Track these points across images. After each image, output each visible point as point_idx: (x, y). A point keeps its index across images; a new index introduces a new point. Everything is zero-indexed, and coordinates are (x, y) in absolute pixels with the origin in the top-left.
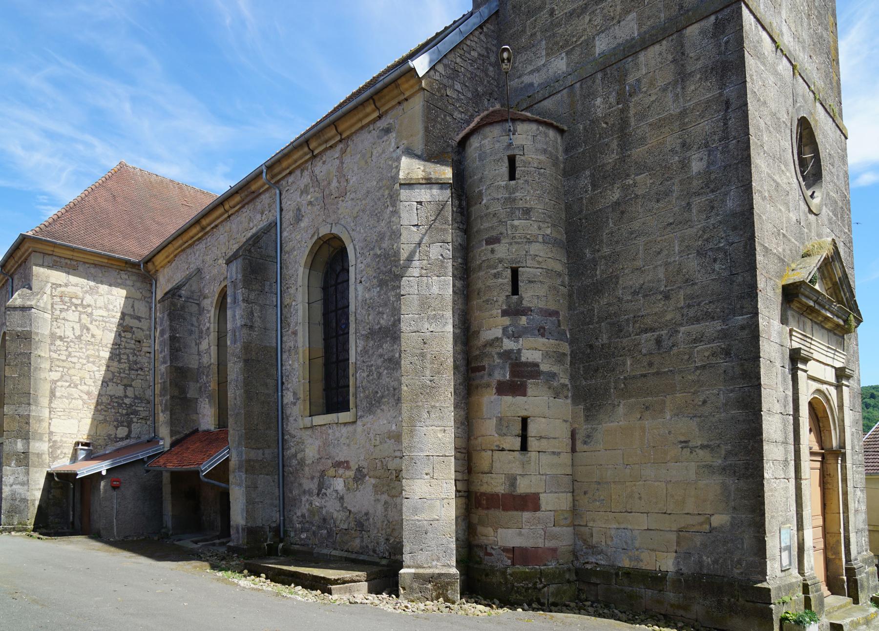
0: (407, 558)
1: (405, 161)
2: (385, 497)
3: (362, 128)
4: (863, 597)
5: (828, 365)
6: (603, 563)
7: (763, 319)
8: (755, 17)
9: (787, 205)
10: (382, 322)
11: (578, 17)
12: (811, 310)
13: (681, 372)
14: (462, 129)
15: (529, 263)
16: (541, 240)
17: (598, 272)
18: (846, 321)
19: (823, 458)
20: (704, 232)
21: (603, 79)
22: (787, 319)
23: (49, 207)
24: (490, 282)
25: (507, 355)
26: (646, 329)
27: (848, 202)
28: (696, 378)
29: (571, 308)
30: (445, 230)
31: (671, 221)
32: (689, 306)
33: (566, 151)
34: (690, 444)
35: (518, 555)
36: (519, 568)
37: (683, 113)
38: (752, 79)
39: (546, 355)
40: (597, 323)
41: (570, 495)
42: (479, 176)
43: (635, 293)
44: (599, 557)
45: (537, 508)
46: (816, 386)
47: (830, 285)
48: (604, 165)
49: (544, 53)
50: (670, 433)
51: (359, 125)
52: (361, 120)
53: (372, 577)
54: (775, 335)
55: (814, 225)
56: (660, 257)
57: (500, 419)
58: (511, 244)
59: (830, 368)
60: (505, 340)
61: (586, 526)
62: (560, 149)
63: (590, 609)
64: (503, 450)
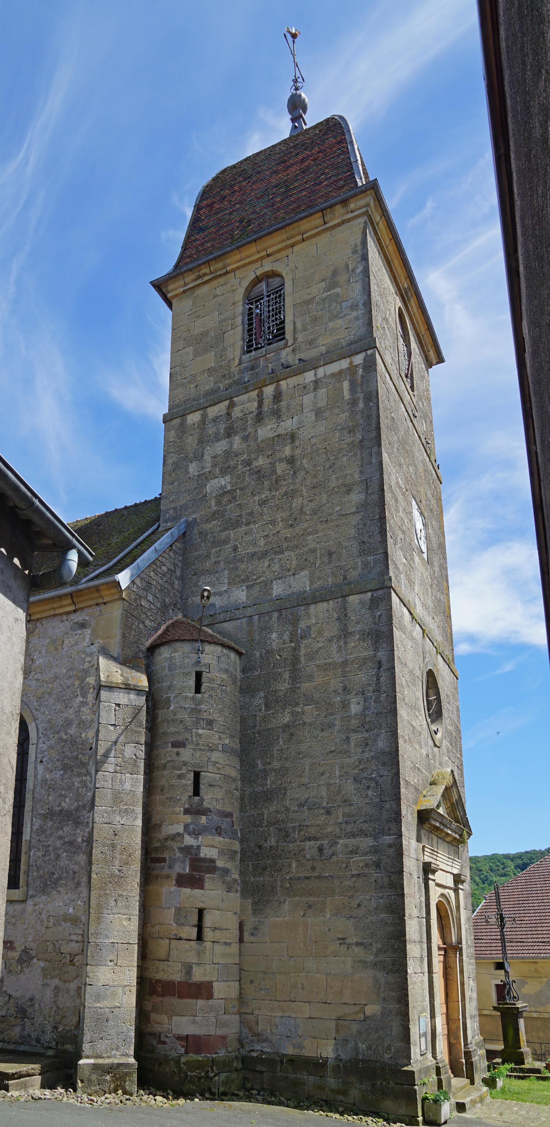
0: (86, 1047)
1: (103, 661)
2: (56, 981)
3: (54, 616)
4: (478, 1078)
5: (448, 872)
6: (268, 1050)
7: (405, 839)
8: (399, 598)
9: (420, 743)
10: (63, 804)
11: (259, 560)
12: (437, 829)
13: (339, 878)
14: (151, 635)
15: (211, 768)
16: (221, 749)
17: (268, 782)
18: (461, 835)
19: (445, 952)
20: (360, 762)
21: (278, 618)
22: (421, 837)
24: (175, 782)
25: (187, 850)
26: (310, 838)
27: (460, 732)
28: (352, 884)
29: (242, 809)
30: (139, 732)
31: (333, 749)
32: (347, 823)
33: (243, 671)
34: (347, 941)
35: (193, 1043)
36: (193, 1057)
37: (345, 663)
38: (398, 647)
39: (222, 852)
40: (266, 827)
41: (237, 983)
42: (168, 683)
43: (301, 805)
44: (264, 1044)
45: (210, 996)
46: (440, 891)
47: (449, 805)
48: (276, 691)
49: (226, 581)
50: (329, 930)
51: (52, 612)
52: (54, 609)
53: (45, 1070)
54: (414, 851)
55: (437, 756)
56: (323, 777)
57: (178, 910)
58: (195, 750)
59: (449, 875)
60: (186, 837)
61: (252, 1014)
62: (238, 669)
63: (259, 1097)
64: (180, 939)
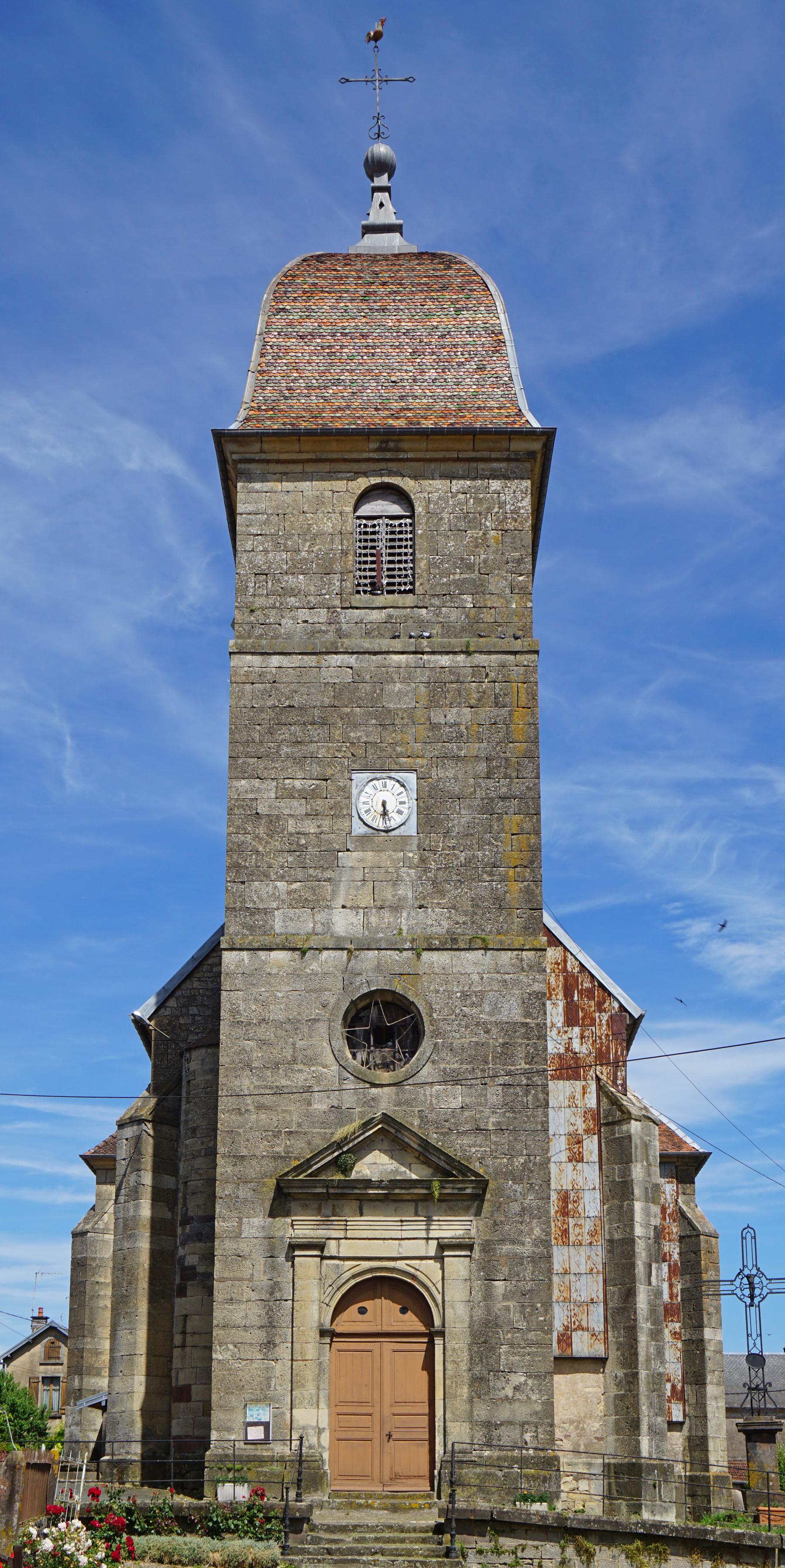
23: (687, 922)
45: (188, 1399)
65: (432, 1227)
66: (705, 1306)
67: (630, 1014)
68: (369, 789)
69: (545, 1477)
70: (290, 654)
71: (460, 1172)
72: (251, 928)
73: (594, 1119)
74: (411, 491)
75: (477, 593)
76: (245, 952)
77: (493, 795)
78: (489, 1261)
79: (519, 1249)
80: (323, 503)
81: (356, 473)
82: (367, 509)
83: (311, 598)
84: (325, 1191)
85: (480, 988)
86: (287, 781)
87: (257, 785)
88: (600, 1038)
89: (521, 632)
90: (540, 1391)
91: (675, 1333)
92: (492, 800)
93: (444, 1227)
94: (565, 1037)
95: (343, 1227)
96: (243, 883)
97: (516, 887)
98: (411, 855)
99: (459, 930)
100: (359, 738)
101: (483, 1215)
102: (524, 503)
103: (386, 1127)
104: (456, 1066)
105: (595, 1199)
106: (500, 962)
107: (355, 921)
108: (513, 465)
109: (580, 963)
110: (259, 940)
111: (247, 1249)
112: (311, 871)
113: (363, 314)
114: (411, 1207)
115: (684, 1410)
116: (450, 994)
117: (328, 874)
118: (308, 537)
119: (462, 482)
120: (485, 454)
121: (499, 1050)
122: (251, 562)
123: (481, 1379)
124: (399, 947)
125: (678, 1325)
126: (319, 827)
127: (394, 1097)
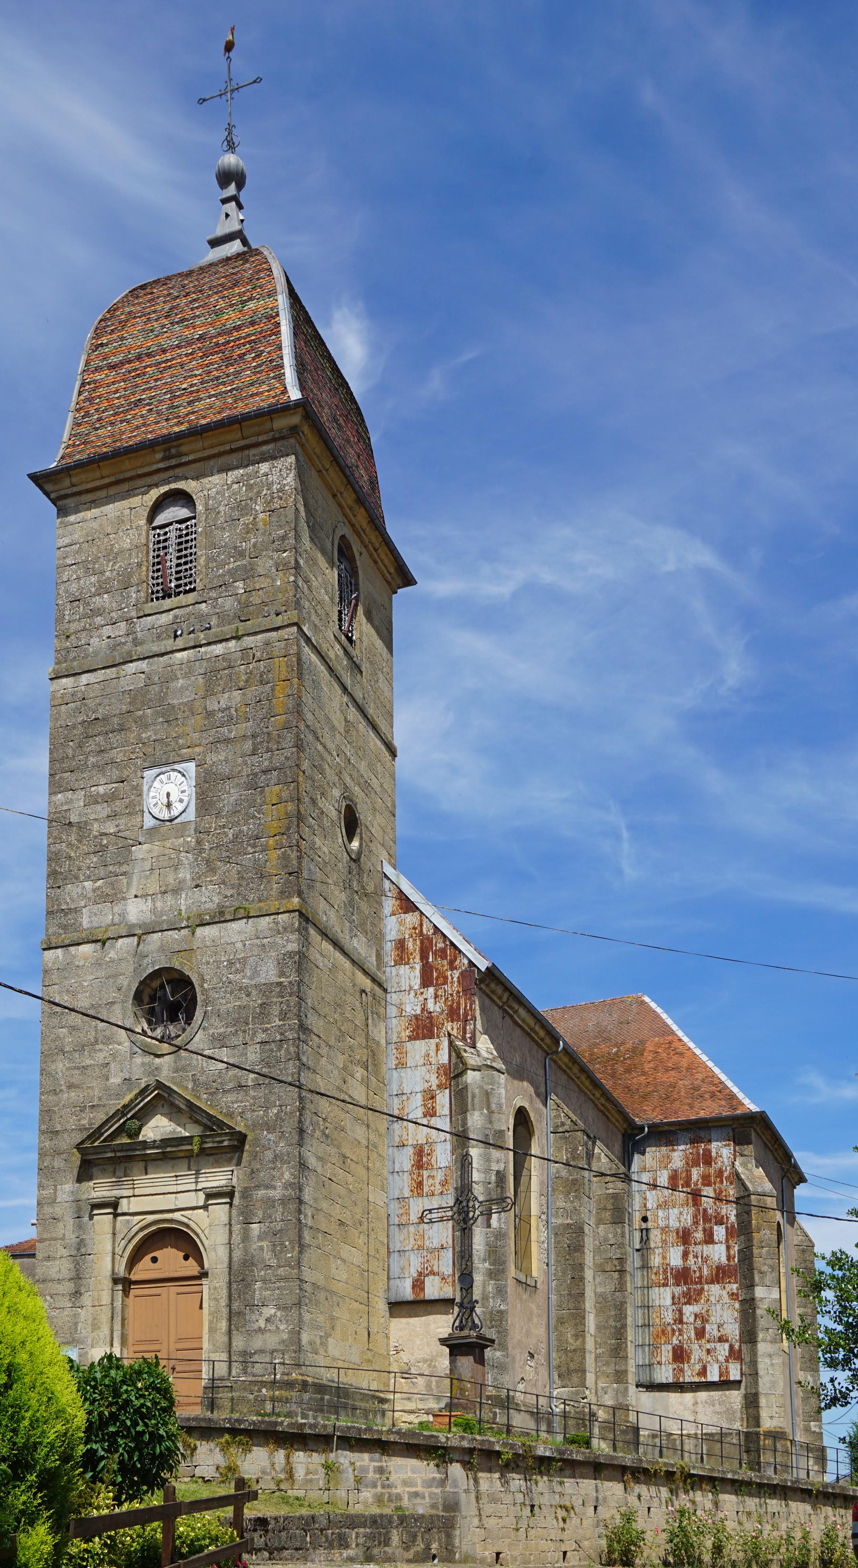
65: (200, 1180)
66: (755, 1265)
67: (478, 968)
68: (156, 784)
69: (287, 1399)
70: (95, 670)
71: (218, 1126)
72: (65, 927)
73: (446, 1074)
74: (193, 492)
75: (248, 578)
76: (60, 950)
77: (257, 770)
78: (247, 1206)
79: (272, 1193)
80: (123, 521)
81: (149, 486)
82: (160, 520)
83: (114, 614)
84: (113, 1155)
85: (243, 955)
86: (93, 789)
87: (70, 796)
88: (452, 995)
89: (284, 608)
90: (287, 1321)
91: (733, 1294)
92: (256, 775)
93: (210, 1179)
94: (421, 998)
95: (131, 1186)
96: (59, 887)
97: (274, 855)
98: (189, 839)
99: (227, 904)
100: (149, 738)
101: (243, 1164)
102: (289, 480)
103: (161, 1092)
104: (222, 1030)
105: (446, 1150)
106: (260, 928)
107: (144, 908)
108: (280, 443)
109: (434, 925)
110: (67, 938)
111: (61, 1212)
112: (111, 868)
113: (165, 330)
114: (185, 1163)
115: (741, 1369)
116: (218, 963)
117: (124, 868)
118: (111, 558)
119: (236, 472)
120: (253, 440)
121: (258, 1010)
122: (67, 592)
123: (239, 1313)
124: (177, 926)
125: (735, 1286)
126: (117, 826)
127: (173, 1064)
